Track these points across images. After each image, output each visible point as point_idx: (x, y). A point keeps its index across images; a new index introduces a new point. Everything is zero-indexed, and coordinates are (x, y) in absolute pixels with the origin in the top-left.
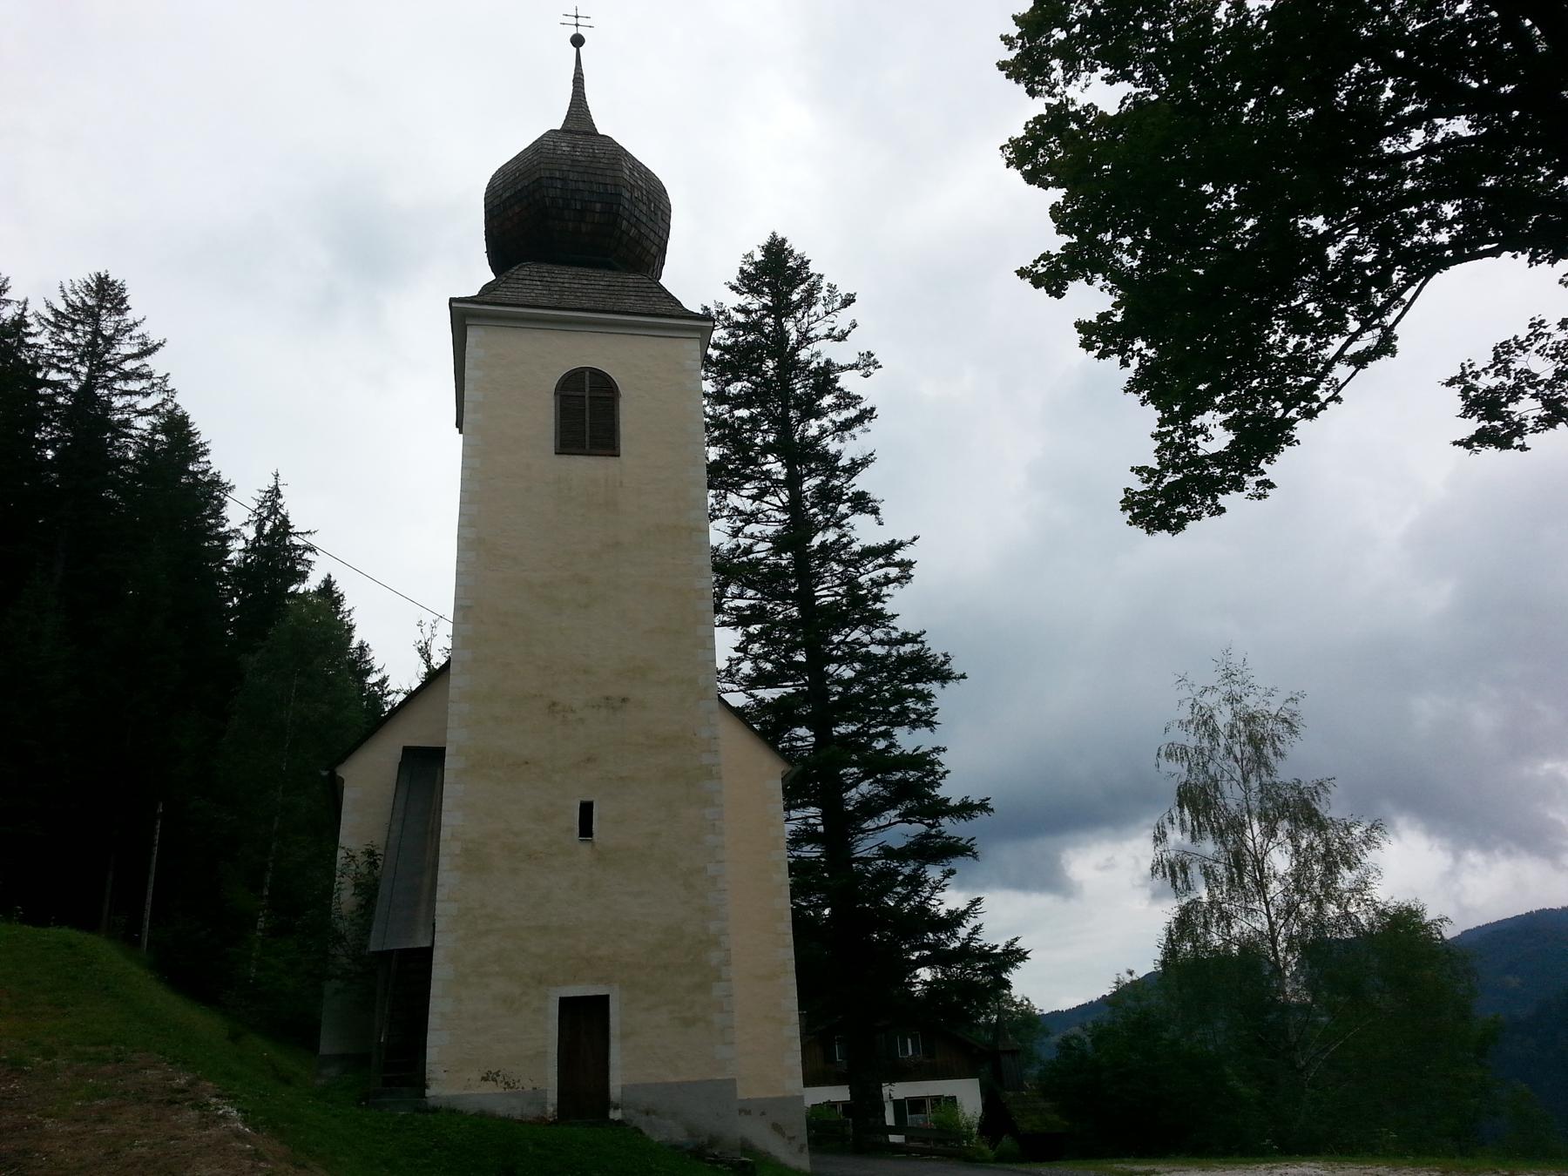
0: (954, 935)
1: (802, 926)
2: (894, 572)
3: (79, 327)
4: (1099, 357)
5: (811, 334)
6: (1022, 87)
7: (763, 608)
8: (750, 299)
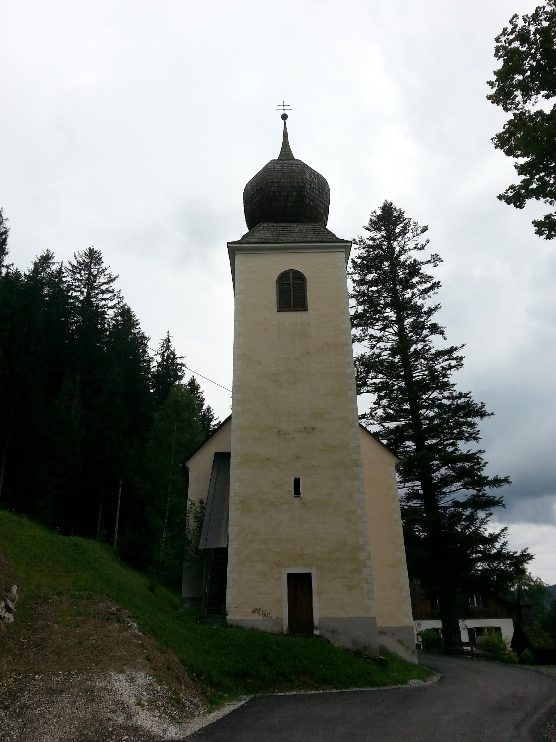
0: (494, 546)
1: (410, 539)
2: (453, 363)
3: (82, 272)
4: (546, 238)
5: (406, 248)
6: (501, 107)
7: (387, 383)
8: (375, 233)
